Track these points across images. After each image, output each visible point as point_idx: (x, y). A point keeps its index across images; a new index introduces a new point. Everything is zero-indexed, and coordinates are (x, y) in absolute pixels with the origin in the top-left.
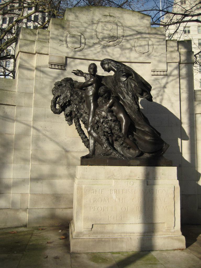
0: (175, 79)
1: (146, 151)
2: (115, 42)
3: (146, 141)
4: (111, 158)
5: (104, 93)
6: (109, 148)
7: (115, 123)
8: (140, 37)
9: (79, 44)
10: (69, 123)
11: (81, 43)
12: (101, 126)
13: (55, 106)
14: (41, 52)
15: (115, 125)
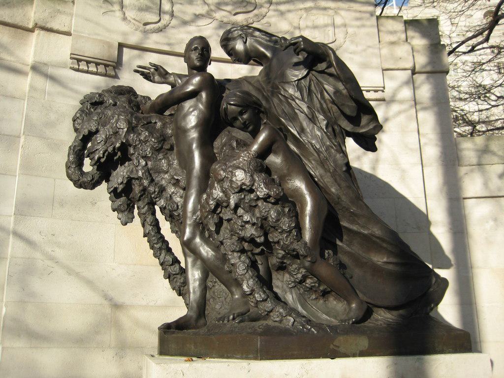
0: (405, 111)
1: (379, 303)
2: (251, 15)
3: (376, 270)
4: (268, 332)
5: (239, 109)
6: (258, 296)
7: (279, 207)
8: (312, 8)
9: (155, 13)
10: (123, 216)
11: (160, 12)
12: (229, 220)
13: (80, 164)
14: (49, 26)
15: (279, 214)
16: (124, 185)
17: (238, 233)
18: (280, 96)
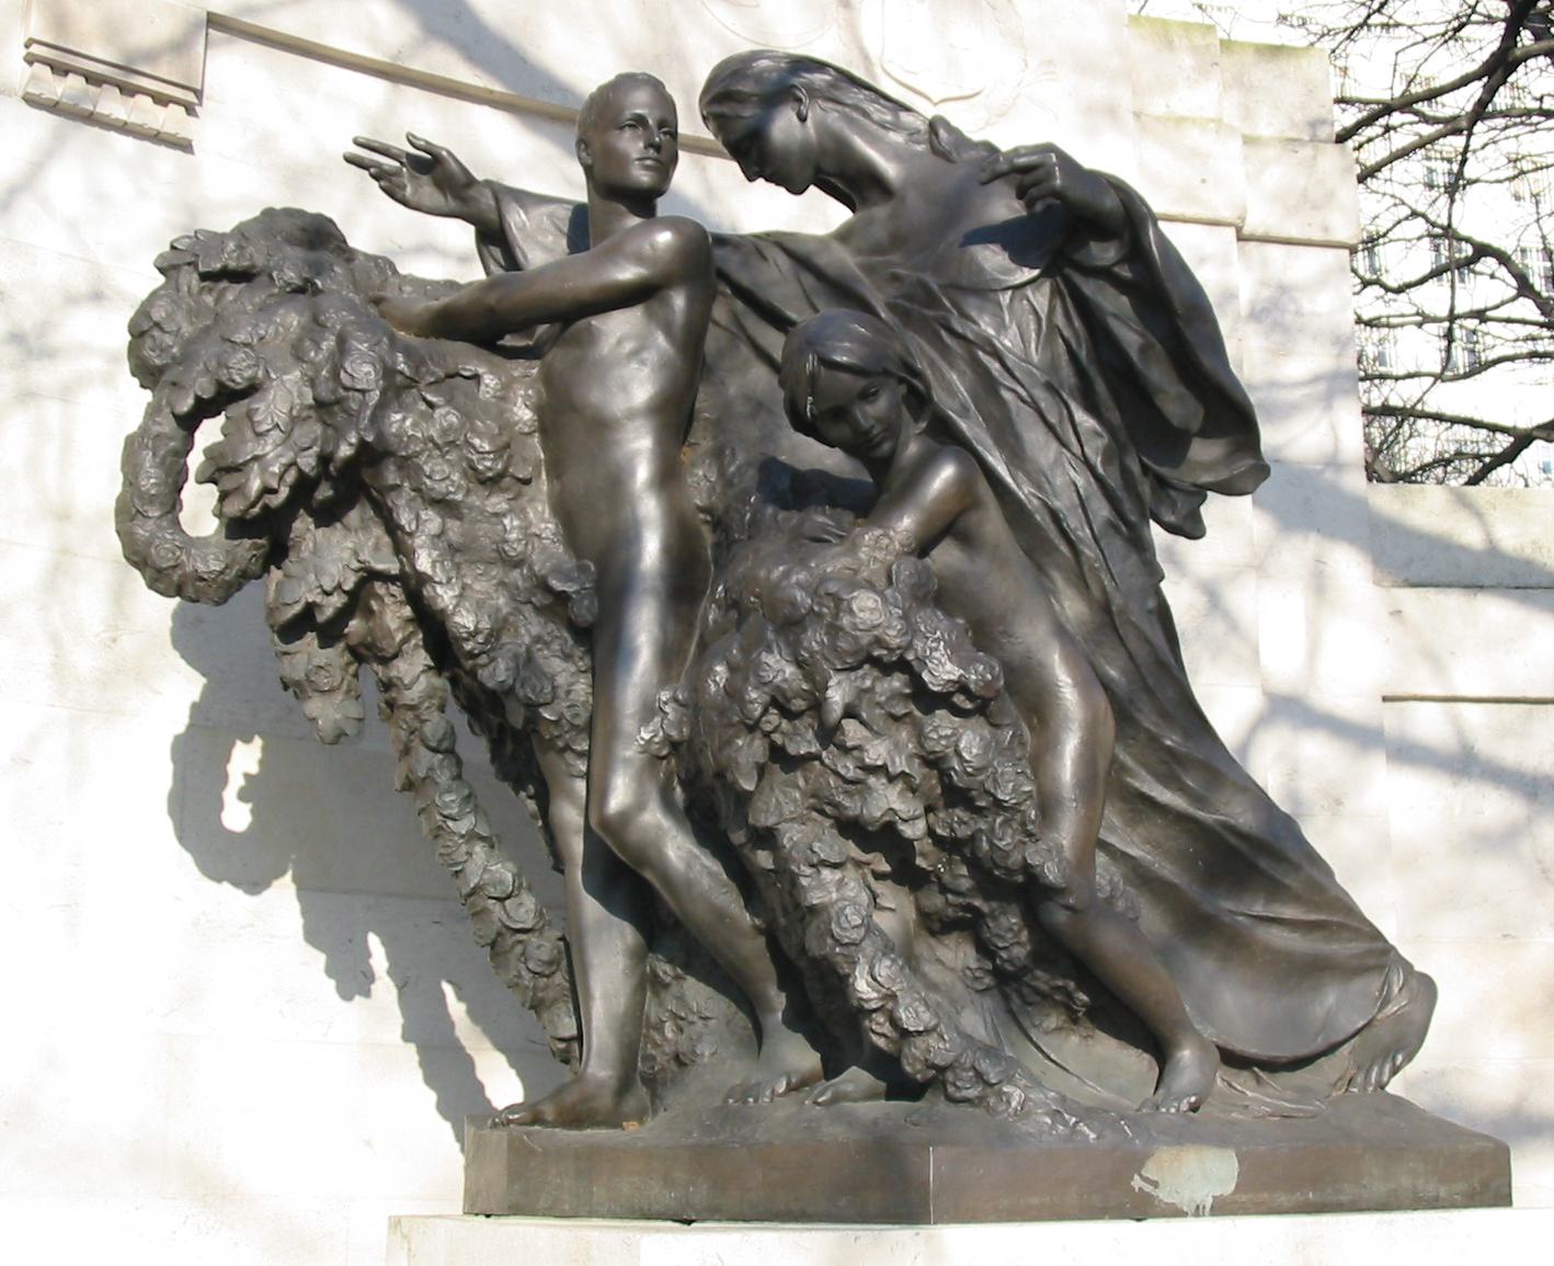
16: (344, 599)
17: (836, 806)
18: (944, 334)
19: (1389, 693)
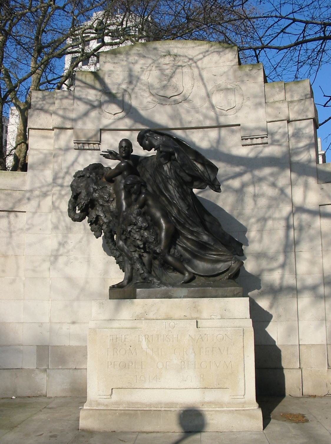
19: (320, 204)
